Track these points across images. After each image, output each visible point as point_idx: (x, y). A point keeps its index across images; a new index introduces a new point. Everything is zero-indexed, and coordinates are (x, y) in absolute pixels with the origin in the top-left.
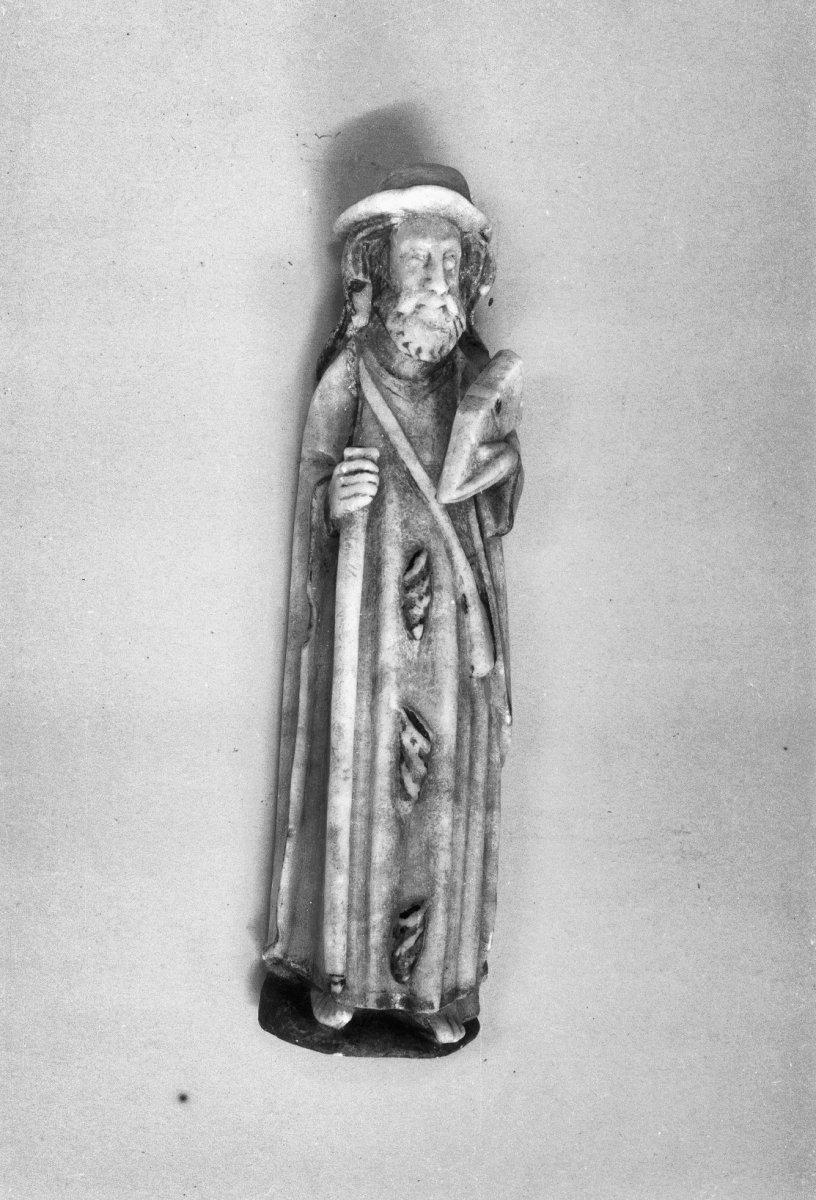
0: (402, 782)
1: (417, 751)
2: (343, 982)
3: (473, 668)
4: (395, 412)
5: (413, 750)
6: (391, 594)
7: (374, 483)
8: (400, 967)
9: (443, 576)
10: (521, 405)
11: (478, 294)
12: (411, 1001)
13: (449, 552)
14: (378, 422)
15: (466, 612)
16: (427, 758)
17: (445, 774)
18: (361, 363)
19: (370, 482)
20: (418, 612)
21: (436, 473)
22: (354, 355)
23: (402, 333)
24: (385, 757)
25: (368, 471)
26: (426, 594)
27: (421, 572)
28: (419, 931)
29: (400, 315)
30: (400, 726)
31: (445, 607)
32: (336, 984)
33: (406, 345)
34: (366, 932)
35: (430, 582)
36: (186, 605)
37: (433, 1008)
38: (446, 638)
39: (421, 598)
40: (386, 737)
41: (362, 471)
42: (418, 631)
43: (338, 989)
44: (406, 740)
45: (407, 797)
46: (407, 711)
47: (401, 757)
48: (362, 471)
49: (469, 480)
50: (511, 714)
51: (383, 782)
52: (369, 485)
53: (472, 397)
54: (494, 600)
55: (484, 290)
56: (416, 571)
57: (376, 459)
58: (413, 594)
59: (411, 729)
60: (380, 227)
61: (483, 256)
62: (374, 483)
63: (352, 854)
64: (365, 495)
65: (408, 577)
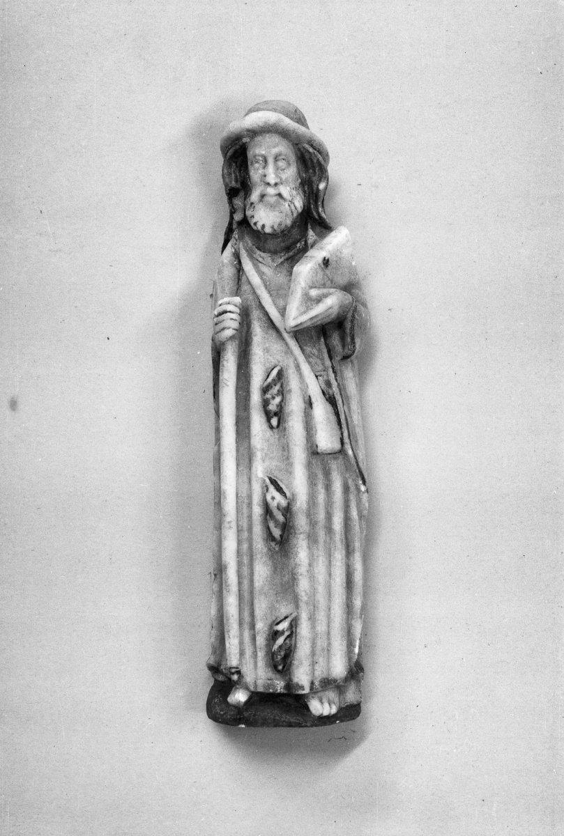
0: (268, 528)
1: (276, 505)
2: (239, 672)
3: (317, 446)
4: (261, 274)
5: (273, 504)
6: (256, 398)
7: (236, 320)
8: (282, 661)
9: (293, 383)
10: (353, 263)
11: (318, 189)
12: (289, 685)
13: (298, 367)
14: (249, 283)
15: (312, 408)
16: (287, 511)
17: (301, 522)
18: (241, 246)
19: (231, 319)
20: (273, 407)
21: (283, 312)
22: (236, 240)
23: (253, 216)
24: (257, 510)
25: (230, 312)
26: (278, 395)
27: (274, 380)
28: (287, 634)
29: (252, 204)
30: (265, 489)
31: (295, 405)
32: (233, 674)
33: (255, 224)
34: (254, 638)
35: (282, 386)
36: (114, 408)
37: (304, 690)
38: (295, 425)
39: (273, 398)
40: (257, 498)
41: (225, 312)
42: (274, 421)
43: (235, 677)
44: (269, 498)
45: (273, 539)
46: (270, 479)
47: (267, 511)
48: (225, 312)
49: (302, 314)
50: (364, 483)
51: (258, 529)
52: (232, 321)
53: (311, 257)
54: (341, 406)
55: (322, 186)
56: (270, 380)
57: (238, 305)
58: (268, 396)
59: (272, 488)
60: (237, 147)
61: (315, 161)
62: (236, 320)
63: (240, 583)
64: (229, 328)
65: (266, 384)
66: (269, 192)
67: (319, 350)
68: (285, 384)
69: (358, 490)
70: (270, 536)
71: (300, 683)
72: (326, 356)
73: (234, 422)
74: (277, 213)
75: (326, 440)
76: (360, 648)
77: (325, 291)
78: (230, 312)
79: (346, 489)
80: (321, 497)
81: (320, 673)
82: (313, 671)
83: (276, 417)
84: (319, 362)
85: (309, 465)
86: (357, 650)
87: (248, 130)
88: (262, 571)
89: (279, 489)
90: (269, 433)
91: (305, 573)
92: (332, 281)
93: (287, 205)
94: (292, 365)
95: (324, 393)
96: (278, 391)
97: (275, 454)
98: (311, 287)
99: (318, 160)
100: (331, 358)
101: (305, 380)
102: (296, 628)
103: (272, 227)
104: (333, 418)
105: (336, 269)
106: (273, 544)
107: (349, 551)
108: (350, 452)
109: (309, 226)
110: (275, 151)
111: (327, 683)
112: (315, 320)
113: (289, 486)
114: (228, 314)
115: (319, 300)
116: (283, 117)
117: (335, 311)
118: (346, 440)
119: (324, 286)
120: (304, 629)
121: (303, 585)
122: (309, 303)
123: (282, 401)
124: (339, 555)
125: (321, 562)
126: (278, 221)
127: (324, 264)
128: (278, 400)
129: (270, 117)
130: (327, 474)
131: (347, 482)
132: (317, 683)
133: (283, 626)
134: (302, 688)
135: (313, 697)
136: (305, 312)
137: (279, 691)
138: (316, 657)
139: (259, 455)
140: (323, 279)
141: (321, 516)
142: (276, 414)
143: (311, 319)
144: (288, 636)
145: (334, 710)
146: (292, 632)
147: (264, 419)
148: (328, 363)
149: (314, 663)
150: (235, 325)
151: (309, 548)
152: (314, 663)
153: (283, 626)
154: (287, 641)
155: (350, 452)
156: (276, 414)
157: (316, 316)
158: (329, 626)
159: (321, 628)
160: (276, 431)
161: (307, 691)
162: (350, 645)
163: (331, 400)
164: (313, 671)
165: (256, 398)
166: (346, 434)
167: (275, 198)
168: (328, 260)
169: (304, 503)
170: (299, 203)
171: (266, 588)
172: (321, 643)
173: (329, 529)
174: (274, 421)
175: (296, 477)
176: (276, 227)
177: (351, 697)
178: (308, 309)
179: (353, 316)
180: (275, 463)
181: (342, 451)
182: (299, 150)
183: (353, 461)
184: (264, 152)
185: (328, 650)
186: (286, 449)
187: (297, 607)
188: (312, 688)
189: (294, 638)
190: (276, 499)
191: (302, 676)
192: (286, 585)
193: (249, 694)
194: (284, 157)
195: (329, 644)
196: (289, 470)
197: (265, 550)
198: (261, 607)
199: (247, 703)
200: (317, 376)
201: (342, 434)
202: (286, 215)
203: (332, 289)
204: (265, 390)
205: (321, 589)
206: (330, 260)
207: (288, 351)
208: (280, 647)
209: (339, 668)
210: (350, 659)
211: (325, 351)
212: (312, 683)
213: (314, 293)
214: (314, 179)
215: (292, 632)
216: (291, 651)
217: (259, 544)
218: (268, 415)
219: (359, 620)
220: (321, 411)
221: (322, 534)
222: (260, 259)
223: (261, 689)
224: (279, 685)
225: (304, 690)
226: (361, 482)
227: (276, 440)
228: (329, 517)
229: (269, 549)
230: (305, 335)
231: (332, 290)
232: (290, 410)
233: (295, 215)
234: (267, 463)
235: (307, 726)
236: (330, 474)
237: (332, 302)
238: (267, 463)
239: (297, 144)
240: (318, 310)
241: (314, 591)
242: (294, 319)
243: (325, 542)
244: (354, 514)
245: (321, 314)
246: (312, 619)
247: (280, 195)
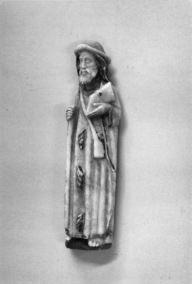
5: (78, 175)
6: (77, 139)
7: (71, 113)
9: (88, 135)
12: (83, 236)
16: (83, 177)
17: (87, 181)
19: (69, 113)
20: (80, 143)
25: (69, 111)
26: (82, 138)
28: (81, 218)
31: (88, 142)
37: (86, 237)
39: (81, 139)
59: (79, 170)
61: (101, 60)
66: (99, 69)
67: (100, 124)
68: (85, 135)
69: (112, 171)
70: (78, 186)
71: (85, 235)
72: (102, 125)
73: (70, 147)
74: (85, 78)
75: (98, 153)
76: (109, 225)
77: (99, 104)
78: (69, 111)
79: (107, 171)
80: (96, 173)
81: (93, 231)
82: (90, 232)
83: (83, 145)
84: (100, 128)
85: (91, 162)
86: (108, 225)
87: (79, 50)
88: (75, 197)
89: (81, 170)
90: (80, 151)
91: (88, 198)
92: (103, 100)
93: (89, 75)
94: (89, 128)
95: (99, 138)
96: (82, 137)
97: (82, 158)
98: (94, 102)
99: (102, 60)
100: (104, 126)
101: (93, 134)
102: (85, 217)
103: (84, 82)
104: (102, 147)
105: (105, 96)
106: (78, 188)
107: (107, 191)
108: (108, 158)
109: (102, 82)
110: (85, 57)
111: (97, 236)
112: (95, 113)
113: (85, 169)
114: (69, 111)
115: (97, 107)
116: (87, 46)
117: (103, 110)
118: (107, 154)
119: (100, 102)
120: (87, 217)
121: (87, 202)
122: (93, 108)
123: (84, 140)
124: (103, 193)
125: (95, 195)
126: (86, 80)
127: (99, 94)
128: (82, 140)
129: (84, 46)
130: (99, 165)
131: (108, 168)
132: (91, 236)
133: (80, 215)
134: (86, 237)
135: (90, 240)
136: (91, 111)
137: (80, 237)
138: (92, 227)
139: (76, 158)
140: (99, 99)
141: (96, 179)
142: (81, 145)
143: (94, 113)
144: (81, 219)
145: (97, 245)
146: (83, 218)
147: (78, 146)
148: (103, 128)
149: (91, 229)
150: (71, 115)
151: (90, 190)
152: (91, 229)
153: (80, 215)
154: (81, 221)
155: (108, 158)
156: (81, 145)
157: (95, 112)
158: (98, 217)
159: (94, 217)
160: (82, 150)
161: (87, 238)
162: (105, 223)
163: (102, 141)
164: (90, 232)
165: (77, 139)
166: (106, 152)
167: (85, 73)
168: (101, 93)
169: (88, 175)
170: (94, 74)
171: (77, 203)
172: (94, 222)
173: (99, 184)
174: (81, 147)
175: (86, 166)
176: (85, 82)
177: (108, 240)
178: (93, 110)
179: (112, 113)
180: (81, 161)
181: (105, 157)
182: (95, 56)
183: (109, 161)
184: (81, 58)
185: (97, 225)
186: (84, 156)
187: (85, 210)
188: (89, 237)
189: (83, 220)
190: (80, 173)
191: (86, 233)
192: (82, 202)
193: (71, 238)
194: (89, 59)
195: (98, 223)
196: (84, 163)
197: (76, 190)
198: (75, 208)
199: (70, 240)
200: (97, 132)
201: (105, 152)
202: (89, 78)
203: (102, 103)
204: (79, 136)
205: (94, 204)
206: (102, 93)
207: (88, 124)
208: (78, 223)
209: (101, 231)
210: (106, 228)
211: (102, 124)
212: (89, 236)
213: (95, 104)
214: (102, 66)
215: (83, 218)
216: (82, 224)
217: (75, 188)
218: (80, 145)
219: (109, 215)
220: (97, 144)
221: (96, 186)
222: (84, 93)
223: (74, 236)
224: (80, 236)
225: (86, 237)
226: (112, 168)
227: (82, 153)
228: (99, 179)
229: (78, 190)
230: (93, 118)
231: (103, 103)
232: (86, 143)
233: (92, 78)
234: (79, 161)
235: (87, 250)
236: (101, 165)
237: (102, 107)
238: (79, 161)
239: (94, 55)
240: (96, 110)
241: (91, 205)
242: (87, 113)
243: (97, 188)
244: (110, 179)
245: (97, 111)
246: (91, 214)
247: (86, 72)
